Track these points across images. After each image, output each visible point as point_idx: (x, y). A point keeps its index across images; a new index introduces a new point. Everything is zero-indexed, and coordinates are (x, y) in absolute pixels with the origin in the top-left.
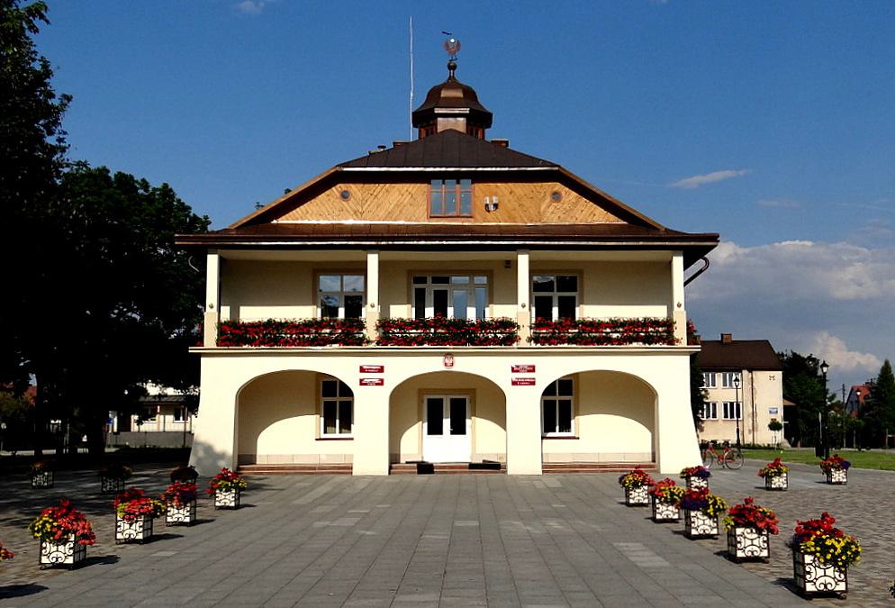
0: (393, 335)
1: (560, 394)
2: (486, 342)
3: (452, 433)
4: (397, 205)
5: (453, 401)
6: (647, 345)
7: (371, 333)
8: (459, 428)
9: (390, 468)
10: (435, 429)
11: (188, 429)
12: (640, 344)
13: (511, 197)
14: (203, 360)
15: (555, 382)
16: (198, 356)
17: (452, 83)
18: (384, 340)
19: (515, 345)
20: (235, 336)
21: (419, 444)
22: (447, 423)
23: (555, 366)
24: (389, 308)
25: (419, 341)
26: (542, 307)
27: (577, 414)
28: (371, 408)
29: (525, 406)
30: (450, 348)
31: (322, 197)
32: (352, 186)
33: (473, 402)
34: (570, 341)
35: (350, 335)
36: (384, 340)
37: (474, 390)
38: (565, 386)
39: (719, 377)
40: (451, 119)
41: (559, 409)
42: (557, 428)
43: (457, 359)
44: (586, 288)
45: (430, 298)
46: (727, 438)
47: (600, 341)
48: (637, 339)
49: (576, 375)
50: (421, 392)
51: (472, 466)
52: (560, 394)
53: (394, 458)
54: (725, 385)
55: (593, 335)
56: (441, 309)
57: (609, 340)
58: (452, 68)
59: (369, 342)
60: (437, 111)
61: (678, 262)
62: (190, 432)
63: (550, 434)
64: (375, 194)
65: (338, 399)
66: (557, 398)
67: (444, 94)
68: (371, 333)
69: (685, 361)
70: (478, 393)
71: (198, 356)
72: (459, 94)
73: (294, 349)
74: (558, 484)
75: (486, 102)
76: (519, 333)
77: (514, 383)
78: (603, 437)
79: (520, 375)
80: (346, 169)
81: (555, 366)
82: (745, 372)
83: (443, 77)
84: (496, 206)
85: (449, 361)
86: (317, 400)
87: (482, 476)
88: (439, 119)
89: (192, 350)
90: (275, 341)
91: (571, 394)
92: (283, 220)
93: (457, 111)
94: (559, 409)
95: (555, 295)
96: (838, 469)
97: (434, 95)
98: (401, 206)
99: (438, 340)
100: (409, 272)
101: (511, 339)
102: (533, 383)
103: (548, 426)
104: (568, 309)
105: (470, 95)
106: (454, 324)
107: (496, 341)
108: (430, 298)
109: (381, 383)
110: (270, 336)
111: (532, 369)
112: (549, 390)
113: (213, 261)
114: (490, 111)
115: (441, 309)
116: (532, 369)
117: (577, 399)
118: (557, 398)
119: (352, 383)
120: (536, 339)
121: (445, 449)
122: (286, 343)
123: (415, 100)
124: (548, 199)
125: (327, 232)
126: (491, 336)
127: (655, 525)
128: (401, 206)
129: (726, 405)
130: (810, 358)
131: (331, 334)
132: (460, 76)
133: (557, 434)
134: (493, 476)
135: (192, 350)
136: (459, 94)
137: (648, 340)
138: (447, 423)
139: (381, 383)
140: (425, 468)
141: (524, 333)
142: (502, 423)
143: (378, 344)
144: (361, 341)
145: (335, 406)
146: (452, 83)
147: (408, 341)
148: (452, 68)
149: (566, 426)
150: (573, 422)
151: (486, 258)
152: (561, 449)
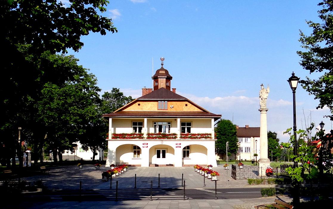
0: (150, 136)
1: (185, 151)
2: (170, 138)
3: (163, 158)
4: (151, 107)
5: (163, 150)
6: (205, 139)
7: (145, 136)
8: (164, 156)
9: (149, 165)
10: (158, 156)
11: (75, 155)
12: (204, 139)
13: (176, 105)
14: (109, 141)
15: (185, 147)
16: (107, 141)
17: (162, 69)
18: (148, 138)
19: (176, 139)
20: (116, 136)
21: (155, 160)
22: (161, 155)
23: (185, 143)
24: (149, 129)
25: (156, 138)
26: (183, 130)
27: (190, 153)
28: (145, 152)
29: (179, 152)
30: (162, 139)
31: (134, 105)
32: (140, 102)
33: (167, 150)
34: (189, 138)
35: (140, 136)
36: (148, 138)
37: (167, 148)
38: (188, 147)
39: (244, 139)
40: (162, 79)
41: (186, 152)
42: (137, 154)
43: (164, 141)
44: (193, 125)
45: (138, 129)
46: (246, 159)
47: (195, 138)
48: (203, 138)
49: (191, 145)
50: (155, 148)
51: (167, 165)
52: (187, 149)
53: (150, 163)
54: (245, 141)
55: (194, 137)
56: (160, 130)
57: (197, 138)
58: (162, 65)
59: (145, 138)
60: (158, 77)
61: (213, 120)
62: (76, 156)
63: (185, 158)
64: (183, 184)
65: (137, 150)
66: (186, 150)
67: (160, 72)
68: (145, 136)
69: (214, 142)
70: (168, 149)
71: (107, 141)
72: (164, 72)
73: (128, 139)
74: (185, 168)
75: (171, 74)
76: (177, 136)
77: (176, 147)
78: (195, 159)
79: (177, 145)
80: (139, 99)
81: (185, 143)
82: (252, 138)
83: (160, 68)
84: (173, 107)
85: (162, 142)
86: (132, 150)
87: (169, 167)
88: (159, 79)
89: (106, 140)
90: (124, 138)
91: (189, 149)
92: (125, 110)
93: (163, 77)
94: (186, 152)
95: (186, 127)
96: (241, 165)
97: (158, 71)
98: (151, 107)
99: (159, 138)
100: (153, 121)
101: (176, 138)
102: (180, 147)
103: (184, 156)
104: (189, 130)
105: (167, 71)
106: (163, 134)
107: (172, 138)
108: (138, 129)
109: (147, 147)
110: (123, 136)
111: (180, 144)
112: (184, 148)
113: (110, 120)
114: (172, 76)
115: (160, 130)
116: (180, 144)
117: (191, 150)
118: (186, 150)
119: (141, 147)
120: (181, 137)
121: (161, 161)
122: (127, 138)
123: (153, 74)
124: (185, 105)
125: (136, 113)
126: (171, 137)
127: (212, 181)
128: (151, 107)
129: (246, 148)
130: (274, 133)
131: (136, 136)
132: (165, 68)
133: (186, 158)
134: (171, 167)
135: (106, 140)
136: (164, 72)
137: (206, 138)
138: (161, 155)
139: (147, 147)
140: (157, 165)
141: (179, 136)
142: (174, 155)
143: (147, 138)
144: (143, 138)
145: (137, 150)
146: (162, 69)
147: (153, 138)
148: (162, 65)
149: (188, 155)
150: (189, 155)
151: (169, 118)
152: (72, 155)
